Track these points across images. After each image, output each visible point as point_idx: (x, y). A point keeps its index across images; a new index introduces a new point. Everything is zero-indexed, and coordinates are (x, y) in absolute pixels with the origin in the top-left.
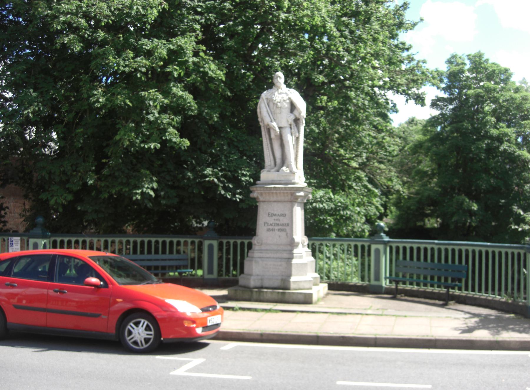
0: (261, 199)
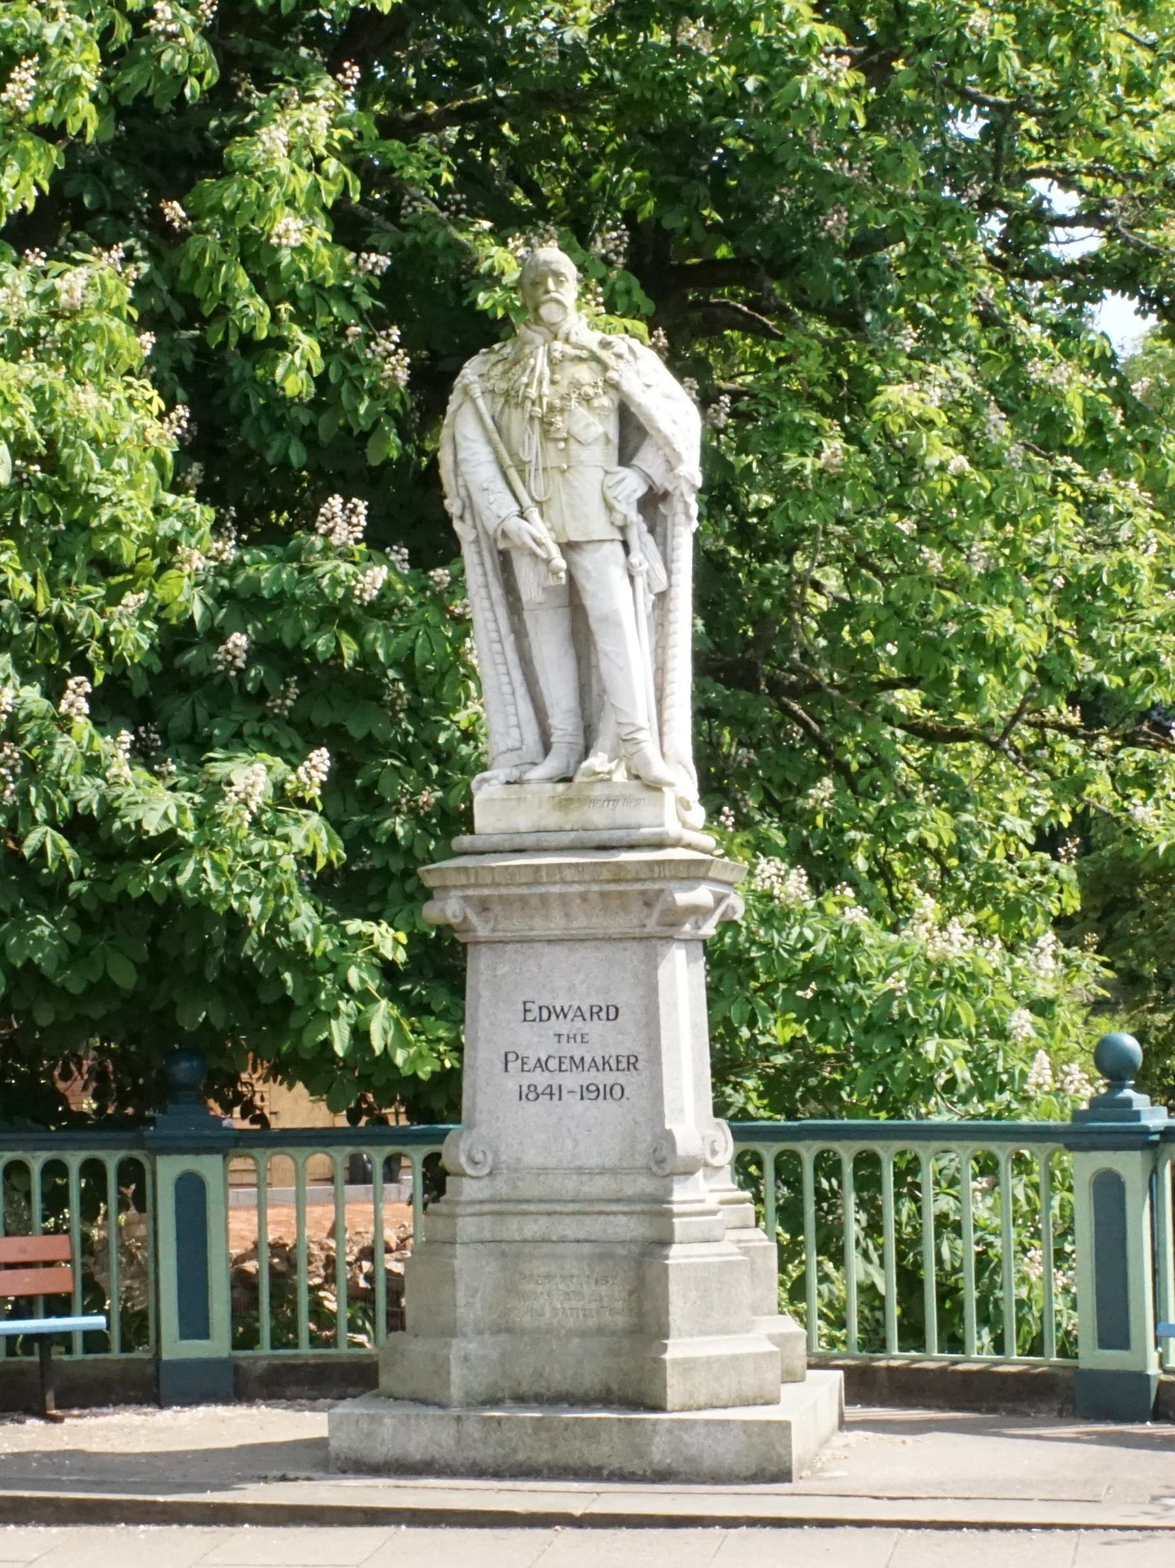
0: (482, 930)
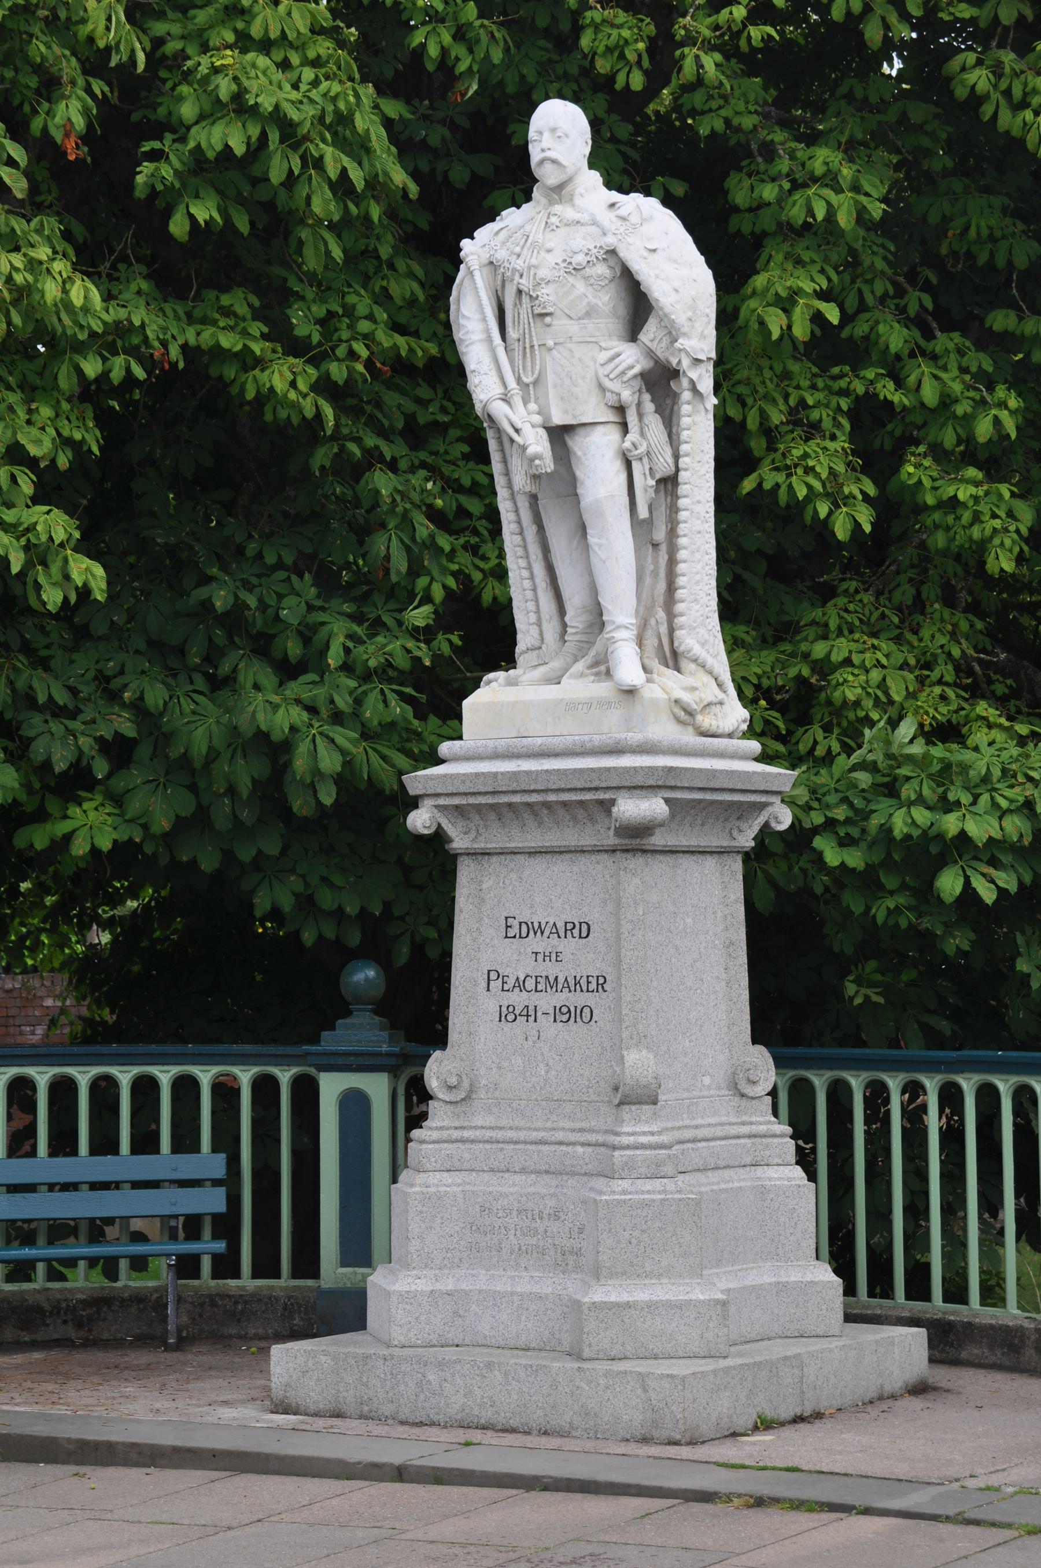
0: (459, 842)
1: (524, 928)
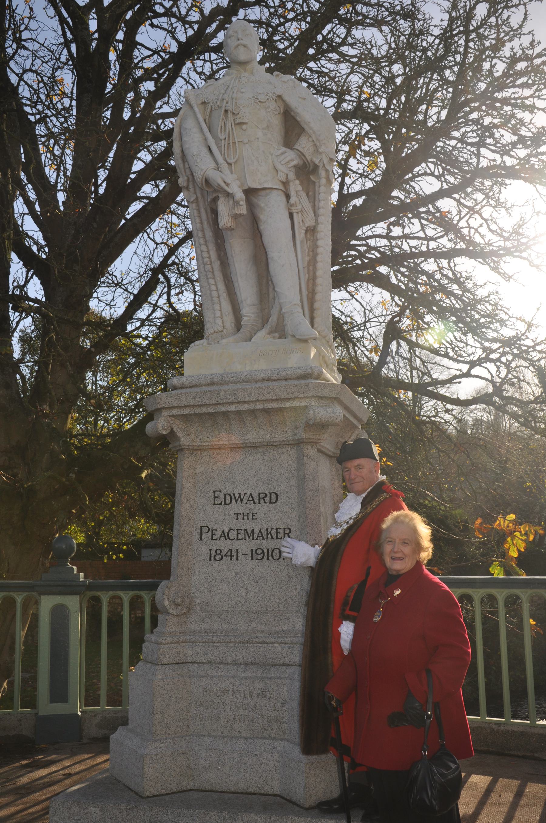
0: (185, 441)
1: (228, 498)
